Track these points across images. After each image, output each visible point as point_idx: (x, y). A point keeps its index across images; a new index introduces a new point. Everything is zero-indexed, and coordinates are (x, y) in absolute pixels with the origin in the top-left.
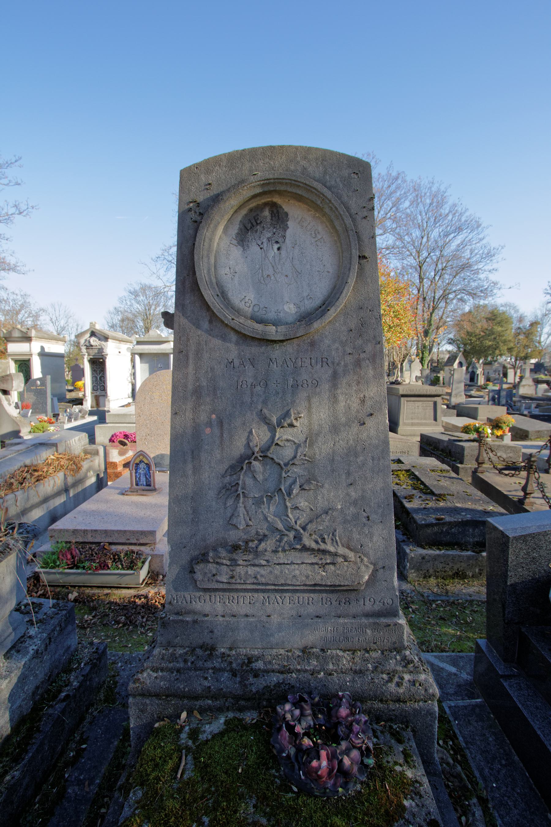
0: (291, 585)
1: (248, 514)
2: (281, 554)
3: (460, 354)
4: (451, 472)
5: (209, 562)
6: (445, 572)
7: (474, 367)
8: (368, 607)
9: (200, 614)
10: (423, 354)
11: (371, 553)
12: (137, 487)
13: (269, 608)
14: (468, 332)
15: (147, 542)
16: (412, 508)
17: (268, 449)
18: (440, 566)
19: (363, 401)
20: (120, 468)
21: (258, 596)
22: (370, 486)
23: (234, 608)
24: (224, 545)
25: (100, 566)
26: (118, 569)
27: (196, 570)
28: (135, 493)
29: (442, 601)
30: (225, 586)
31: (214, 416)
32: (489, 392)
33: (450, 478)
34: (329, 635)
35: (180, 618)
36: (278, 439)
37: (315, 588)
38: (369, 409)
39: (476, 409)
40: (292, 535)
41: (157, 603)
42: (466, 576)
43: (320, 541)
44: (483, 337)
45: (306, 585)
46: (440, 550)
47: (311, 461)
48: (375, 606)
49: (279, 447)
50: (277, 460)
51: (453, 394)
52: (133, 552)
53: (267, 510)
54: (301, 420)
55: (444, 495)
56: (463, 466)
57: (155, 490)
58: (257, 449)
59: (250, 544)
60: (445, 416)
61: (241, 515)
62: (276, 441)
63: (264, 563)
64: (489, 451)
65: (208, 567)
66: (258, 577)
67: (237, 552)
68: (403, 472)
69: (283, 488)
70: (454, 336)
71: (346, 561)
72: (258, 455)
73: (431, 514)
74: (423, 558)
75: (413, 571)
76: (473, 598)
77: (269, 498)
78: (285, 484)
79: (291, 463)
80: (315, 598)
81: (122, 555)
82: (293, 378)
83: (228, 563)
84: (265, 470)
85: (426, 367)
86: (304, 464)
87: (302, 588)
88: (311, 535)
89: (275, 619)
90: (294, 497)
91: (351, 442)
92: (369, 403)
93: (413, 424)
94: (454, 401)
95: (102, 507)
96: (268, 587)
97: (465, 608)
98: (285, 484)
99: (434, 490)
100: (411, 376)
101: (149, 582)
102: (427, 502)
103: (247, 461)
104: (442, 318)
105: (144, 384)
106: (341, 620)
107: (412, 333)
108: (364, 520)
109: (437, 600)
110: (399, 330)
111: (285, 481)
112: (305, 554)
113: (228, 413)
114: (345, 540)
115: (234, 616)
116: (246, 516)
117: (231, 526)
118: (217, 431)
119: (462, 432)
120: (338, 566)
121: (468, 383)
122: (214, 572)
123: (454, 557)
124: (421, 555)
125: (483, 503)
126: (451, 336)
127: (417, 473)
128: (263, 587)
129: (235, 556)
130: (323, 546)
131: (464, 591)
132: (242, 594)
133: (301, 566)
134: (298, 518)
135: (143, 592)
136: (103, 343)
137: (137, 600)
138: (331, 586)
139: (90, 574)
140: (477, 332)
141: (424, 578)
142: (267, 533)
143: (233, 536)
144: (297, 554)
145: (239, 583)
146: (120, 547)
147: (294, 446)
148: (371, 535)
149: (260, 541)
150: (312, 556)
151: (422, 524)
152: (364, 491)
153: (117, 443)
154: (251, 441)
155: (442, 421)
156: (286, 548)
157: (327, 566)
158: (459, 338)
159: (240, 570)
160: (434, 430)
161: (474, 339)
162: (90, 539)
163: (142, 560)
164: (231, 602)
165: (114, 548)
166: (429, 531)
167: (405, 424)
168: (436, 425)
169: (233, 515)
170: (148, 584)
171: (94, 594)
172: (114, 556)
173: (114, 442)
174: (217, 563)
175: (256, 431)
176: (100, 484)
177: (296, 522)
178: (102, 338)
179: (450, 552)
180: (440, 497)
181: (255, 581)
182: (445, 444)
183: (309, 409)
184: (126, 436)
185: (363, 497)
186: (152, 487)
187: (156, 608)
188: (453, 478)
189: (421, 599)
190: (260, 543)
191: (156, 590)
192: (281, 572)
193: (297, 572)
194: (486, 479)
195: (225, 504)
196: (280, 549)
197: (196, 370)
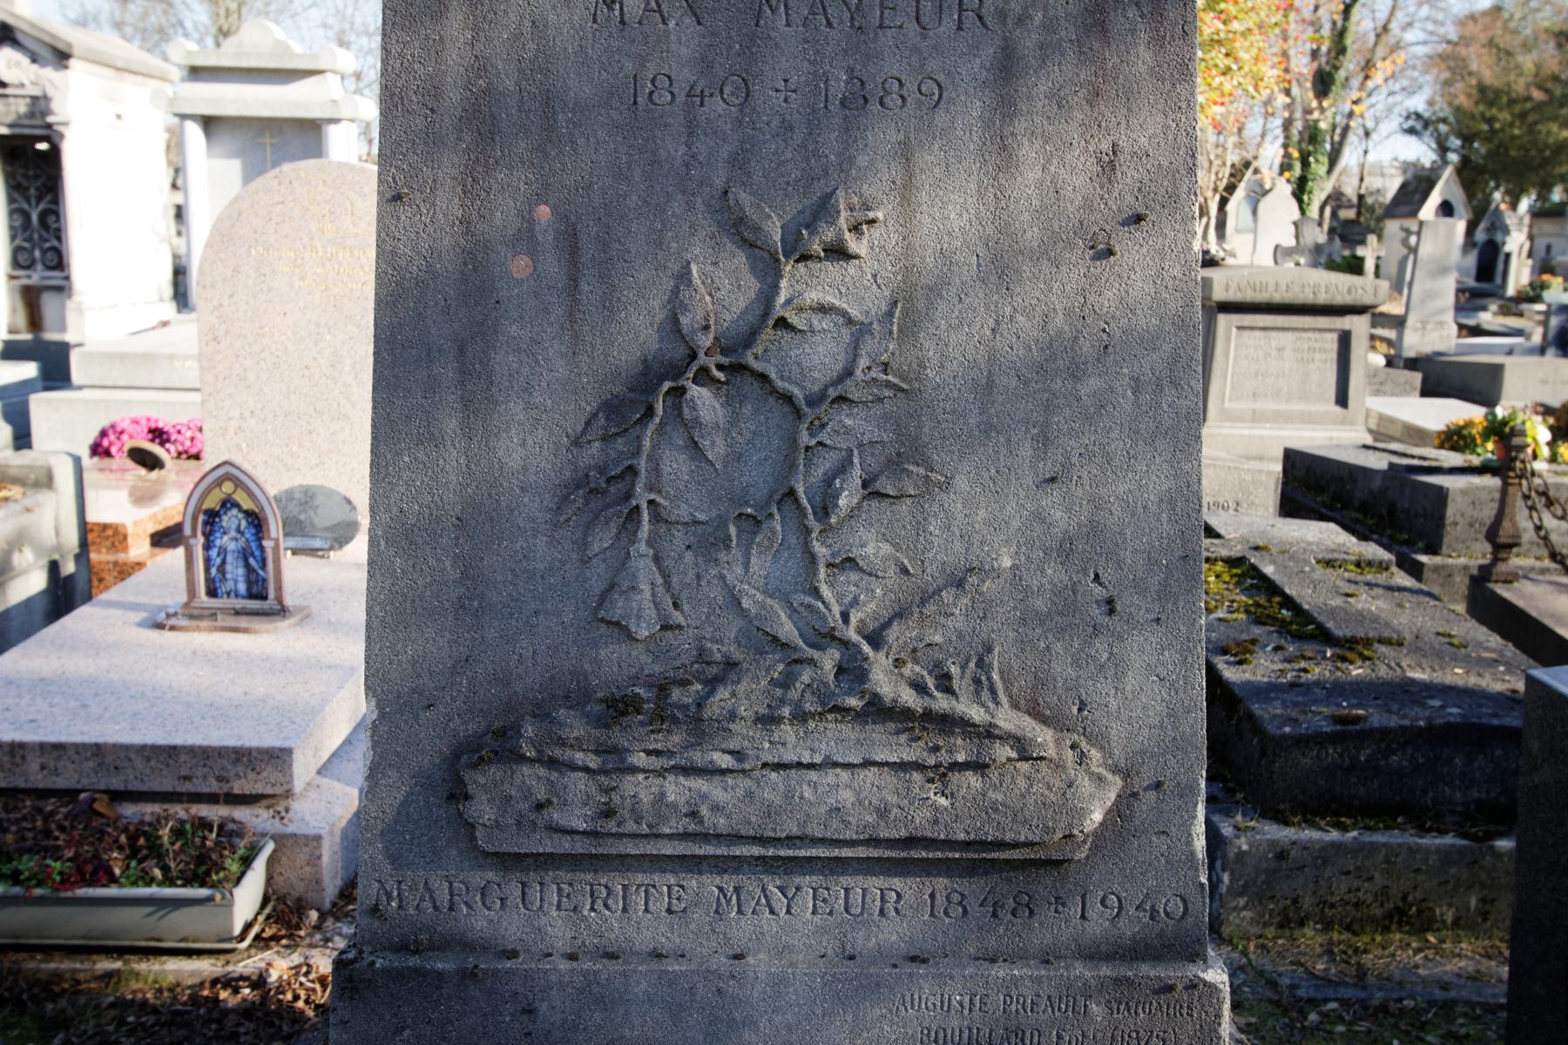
0: (822, 841)
1: (668, 585)
2: (788, 732)
3: (1448, 172)
4: (1394, 569)
5: (522, 759)
6: (1357, 905)
7: (1498, 226)
8: (1098, 924)
9: (485, 949)
10: (1305, 164)
11: (1116, 732)
12: (214, 603)
13: (740, 928)
14: (1482, 89)
15: (259, 789)
16: (1248, 683)
17: (749, 339)
18: (1342, 886)
19: (1108, 166)
20: (139, 548)
21: (701, 885)
22: (1122, 488)
23: (612, 926)
24: (578, 697)
25: (80, 871)
26: (150, 882)
27: (471, 789)
28: (204, 623)
29: (1343, 1002)
30: (581, 846)
31: (544, 212)
32: (1547, 314)
33: (1390, 588)
34: (956, 1023)
35: (415, 961)
36: (788, 302)
37: (909, 855)
38: (1129, 199)
39: (1496, 371)
40: (829, 660)
41: (300, 1004)
42: (1432, 920)
43: (930, 683)
44: (1539, 106)
45: (874, 842)
46: (1343, 828)
47: (905, 389)
48: (1122, 923)
49: (788, 336)
50: (779, 384)
51: (1411, 321)
52: (205, 824)
53: (739, 570)
54: (876, 233)
55: (1368, 642)
56: (1437, 560)
57: (281, 611)
58: (706, 341)
59: (676, 694)
60: (1377, 393)
61: (645, 587)
62: (779, 311)
63: (725, 761)
64: (1540, 502)
65: (518, 779)
66: (704, 811)
67: (625, 720)
68: (1219, 567)
69: (801, 490)
70: (1430, 103)
71: (1024, 758)
72: (711, 363)
73: (1316, 702)
74: (1282, 855)
75: (1242, 902)
76: (1453, 994)
77: (746, 524)
78: (807, 473)
79: (832, 393)
80: (908, 895)
81: (165, 833)
82: (850, 70)
83: (593, 762)
84: (734, 421)
85: (1313, 212)
86: (880, 400)
87: (861, 852)
88: (898, 663)
89: (760, 962)
90: (841, 523)
91: (1059, 319)
92: (1129, 175)
93: (1256, 418)
94: (1415, 342)
95: (78, 665)
96: (737, 851)
97: (1423, 1026)
98: (807, 473)
99: (1330, 625)
100: (1262, 241)
101: (268, 933)
102: (1303, 664)
103: (667, 385)
104: (1385, 28)
105: (223, 234)
106: (1000, 971)
107: (1271, 73)
108: (1096, 612)
109: (1326, 1001)
110: (1223, 62)
111: (809, 464)
112: (877, 732)
113: (597, 201)
114: (1023, 683)
115: (613, 956)
116: (660, 590)
117: (603, 628)
118: (553, 267)
119: (1441, 447)
120: (994, 775)
121: (1471, 282)
122: (541, 794)
123: (1392, 851)
124: (1273, 844)
125: (1509, 671)
126: (1418, 103)
127: (1269, 570)
128: (721, 851)
129: (618, 737)
130: (942, 703)
131: (1421, 971)
132: (640, 878)
133: (863, 773)
134: (855, 602)
135: (248, 965)
136: (49, 74)
137: (224, 995)
138: (966, 845)
139: (41, 901)
140: (1520, 86)
141: (1281, 926)
142: (737, 655)
143: (615, 663)
144: (849, 731)
145: (634, 836)
146: (150, 810)
147: (846, 332)
148: (1118, 666)
149: (712, 684)
150: (903, 738)
151: (1284, 736)
152: (1097, 504)
153: (121, 461)
154: (685, 308)
155: (1368, 413)
156: (808, 707)
157: (955, 777)
158: (1446, 112)
159: (639, 789)
160: (1338, 438)
161: (1505, 116)
162: (39, 780)
163: (241, 852)
164: (599, 905)
165: (130, 811)
166: (1306, 762)
167: (1227, 416)
168: (1344, 421)
169: (612, 586)
170: (261, 942)
171: (57, 976)
172: (133, 838)
173: (107, 453)
174: (553, 763)
175: (703, 273)
176: (63, 595)
177: (845, 617)
178: (45, 53)
179: (1379, 838)
180: (1351, 648)
181: (692, 828)
182: (1377, 484)
183: (906, 192)
184: (159, 435)
185: (1094, 530)
186: (271, 603)
187: (299, 1017)
188: (1401, 589)
189: (1269, 994)
190: (712, 692)
191: (296, 958)
192: (788, 796)
193: (847, 796)
194: (1520, 603)
195: (584, 545)
196: (786, 711)
197: (476, 29)
